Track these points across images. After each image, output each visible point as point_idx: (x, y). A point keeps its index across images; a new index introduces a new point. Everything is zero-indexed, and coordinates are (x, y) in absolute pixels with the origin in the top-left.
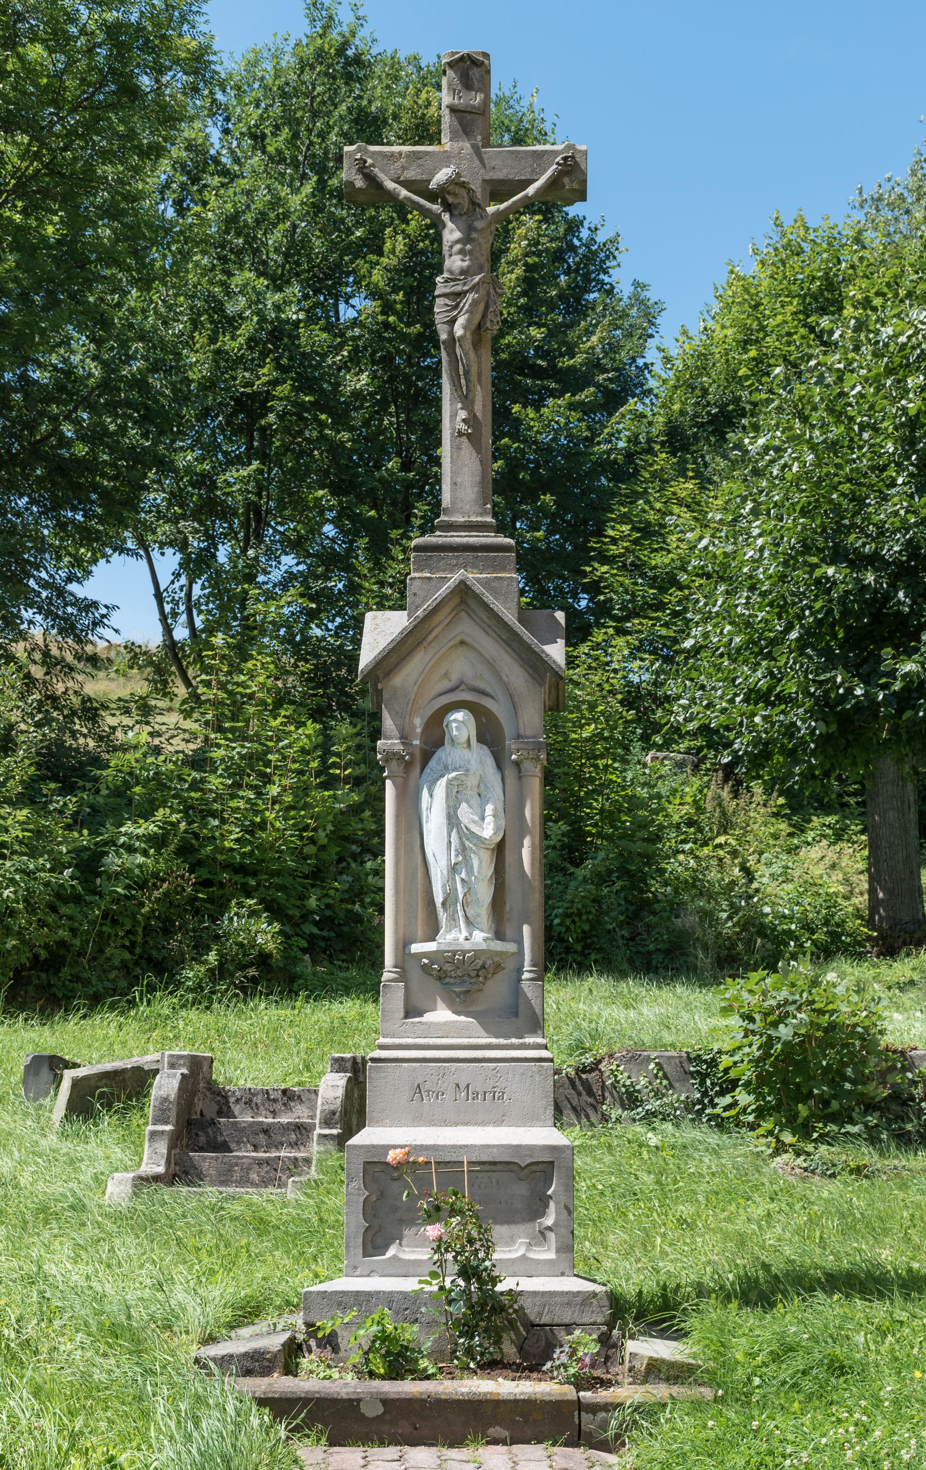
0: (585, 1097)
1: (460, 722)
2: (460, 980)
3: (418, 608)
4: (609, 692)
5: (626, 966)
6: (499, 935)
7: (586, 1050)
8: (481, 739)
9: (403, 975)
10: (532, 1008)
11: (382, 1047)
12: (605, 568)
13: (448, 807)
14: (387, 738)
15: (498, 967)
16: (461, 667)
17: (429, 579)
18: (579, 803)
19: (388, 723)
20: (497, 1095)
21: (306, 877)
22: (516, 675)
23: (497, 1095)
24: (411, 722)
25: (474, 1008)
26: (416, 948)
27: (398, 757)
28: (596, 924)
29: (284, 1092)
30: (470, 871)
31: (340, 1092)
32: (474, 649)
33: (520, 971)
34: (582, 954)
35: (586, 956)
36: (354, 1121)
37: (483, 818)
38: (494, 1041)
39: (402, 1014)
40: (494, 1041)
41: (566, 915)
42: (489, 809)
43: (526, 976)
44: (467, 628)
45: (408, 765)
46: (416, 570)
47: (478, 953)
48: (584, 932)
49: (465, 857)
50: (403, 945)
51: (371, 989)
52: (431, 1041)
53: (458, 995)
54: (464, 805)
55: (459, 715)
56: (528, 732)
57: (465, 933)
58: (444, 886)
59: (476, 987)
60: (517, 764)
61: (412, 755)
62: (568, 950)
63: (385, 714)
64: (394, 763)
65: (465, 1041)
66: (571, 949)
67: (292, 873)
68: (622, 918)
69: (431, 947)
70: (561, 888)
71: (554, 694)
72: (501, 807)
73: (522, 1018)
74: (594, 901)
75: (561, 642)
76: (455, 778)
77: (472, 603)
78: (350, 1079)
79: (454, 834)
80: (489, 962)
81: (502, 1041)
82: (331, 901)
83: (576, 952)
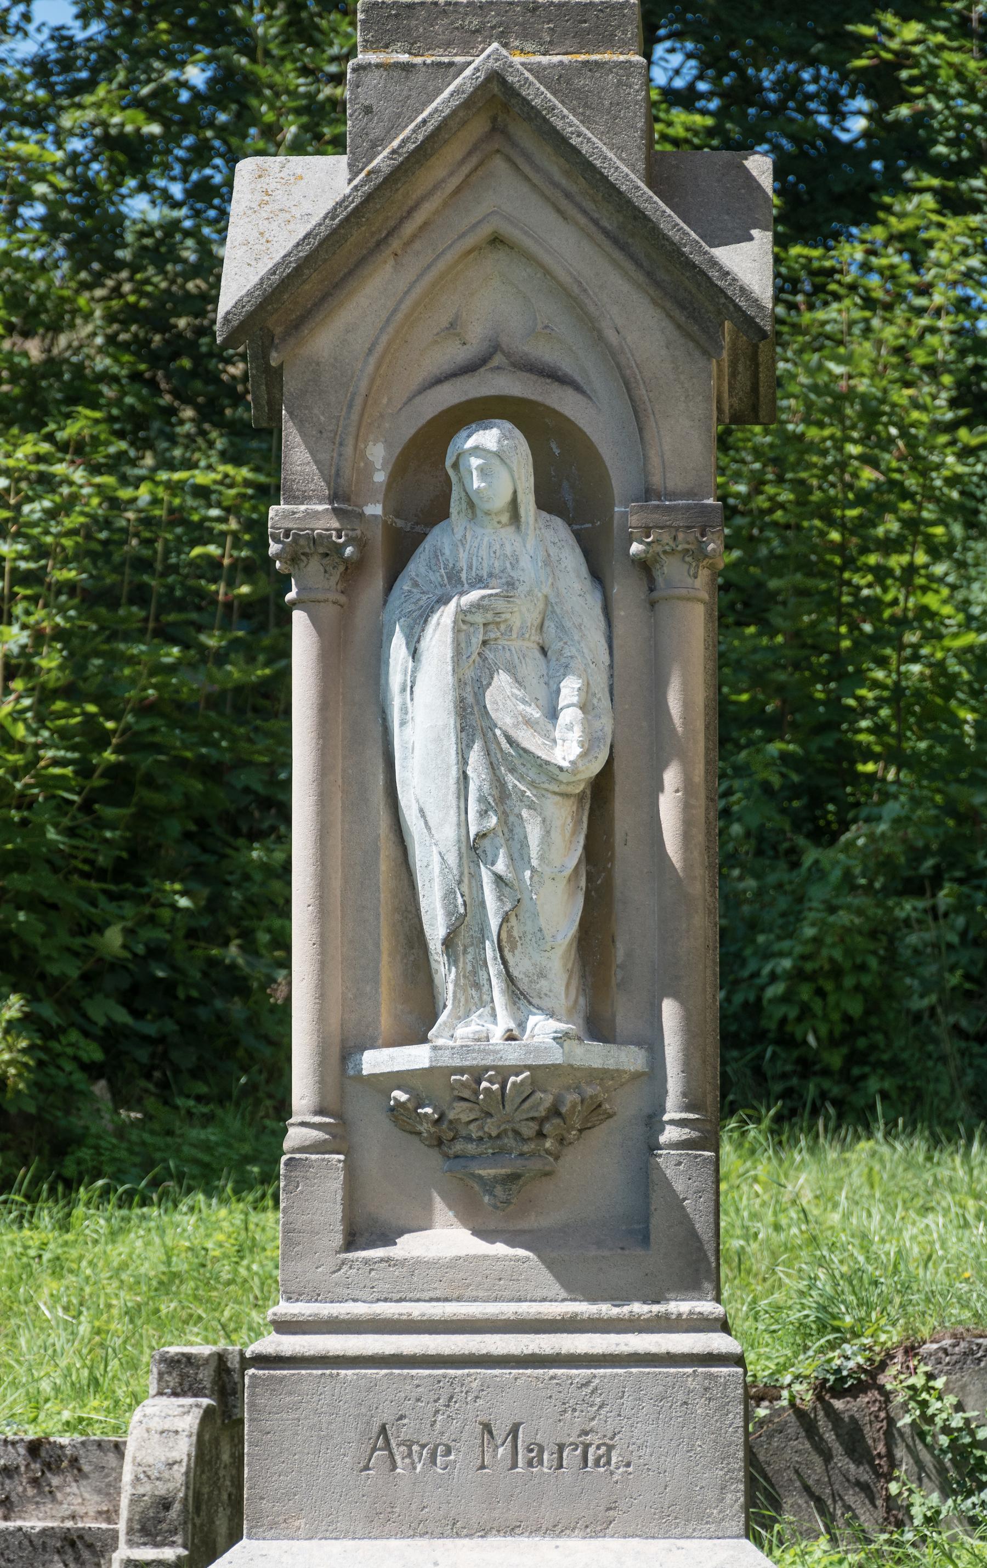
0: (842, 1461)
1: (490, 457)
2: (492, 1146)
3: (375, 146)
4: (926, 368)
5: (962, 1108)
6: (597, 1027)
7: (843, 1336)
8: (548, 500)
9: (340, 1135)
10: (686, 1220)
11: (285, 1326)
12: (912, 30)
13: (460, 683)
14: (294, 499)
15: (596, 1112)
16: (493, 305)
17: (407, 68)
18: (843, 672)
19: (298, 457)
20: (592, 1454)
21: (100, 874)
22: (640, 326)
23: (592, 1454)
24: (360, 454)
25: (532, 1222)
26: (375, 1061)
27: (323, 548)
28: (878, 999)
29: (34, 1448)
30: (519, 857)
31: (183, 1448)
32: (528, 257)
33: (653, 1122)
34: (845, 1076)
35: (855, 1083)
36: (222, 1524)
37: (553, 714)
38: (584, 1308)
39: (338, 1239)
40: (584, 1308)
41: (798, 975)
42: (570, 689)
43: (670, 1134)
44: (508, 200)
45: (353, 572)
46: (370, 46)
47: (541, 1075)
48: (847, 1019)
49: (504, 818)
50: (341, 1053)
51: (252, 1168)
52: (417, 1310)
53: (488, 1185)
54: (502, 679)
55: (487, 438)
56: (675, 481)
57: (505, 1022)
58: (449, 895)
59: (536, 1165)
60: (645, 567)
61: (361, 544)
62: (807, 1066)
63: (291, 435)
64: (314, 567)
65: (508, 1310)
66: (795, 1063)
67: (56, 863)
68: (954, 979)
69: (415, 1057)
70: (783, 903)
71: (744, 378)
72: (600, 682)
73: (661, 1248)
74: (873, 934)
75: (762, 240)
76: (477, 606)
77: (523, 133)
78: (208, 1414)
79: (475, 756)
80: (571, 1098)
81: (606, 1310)
82: (159, 934)
83: (826, 1072)
